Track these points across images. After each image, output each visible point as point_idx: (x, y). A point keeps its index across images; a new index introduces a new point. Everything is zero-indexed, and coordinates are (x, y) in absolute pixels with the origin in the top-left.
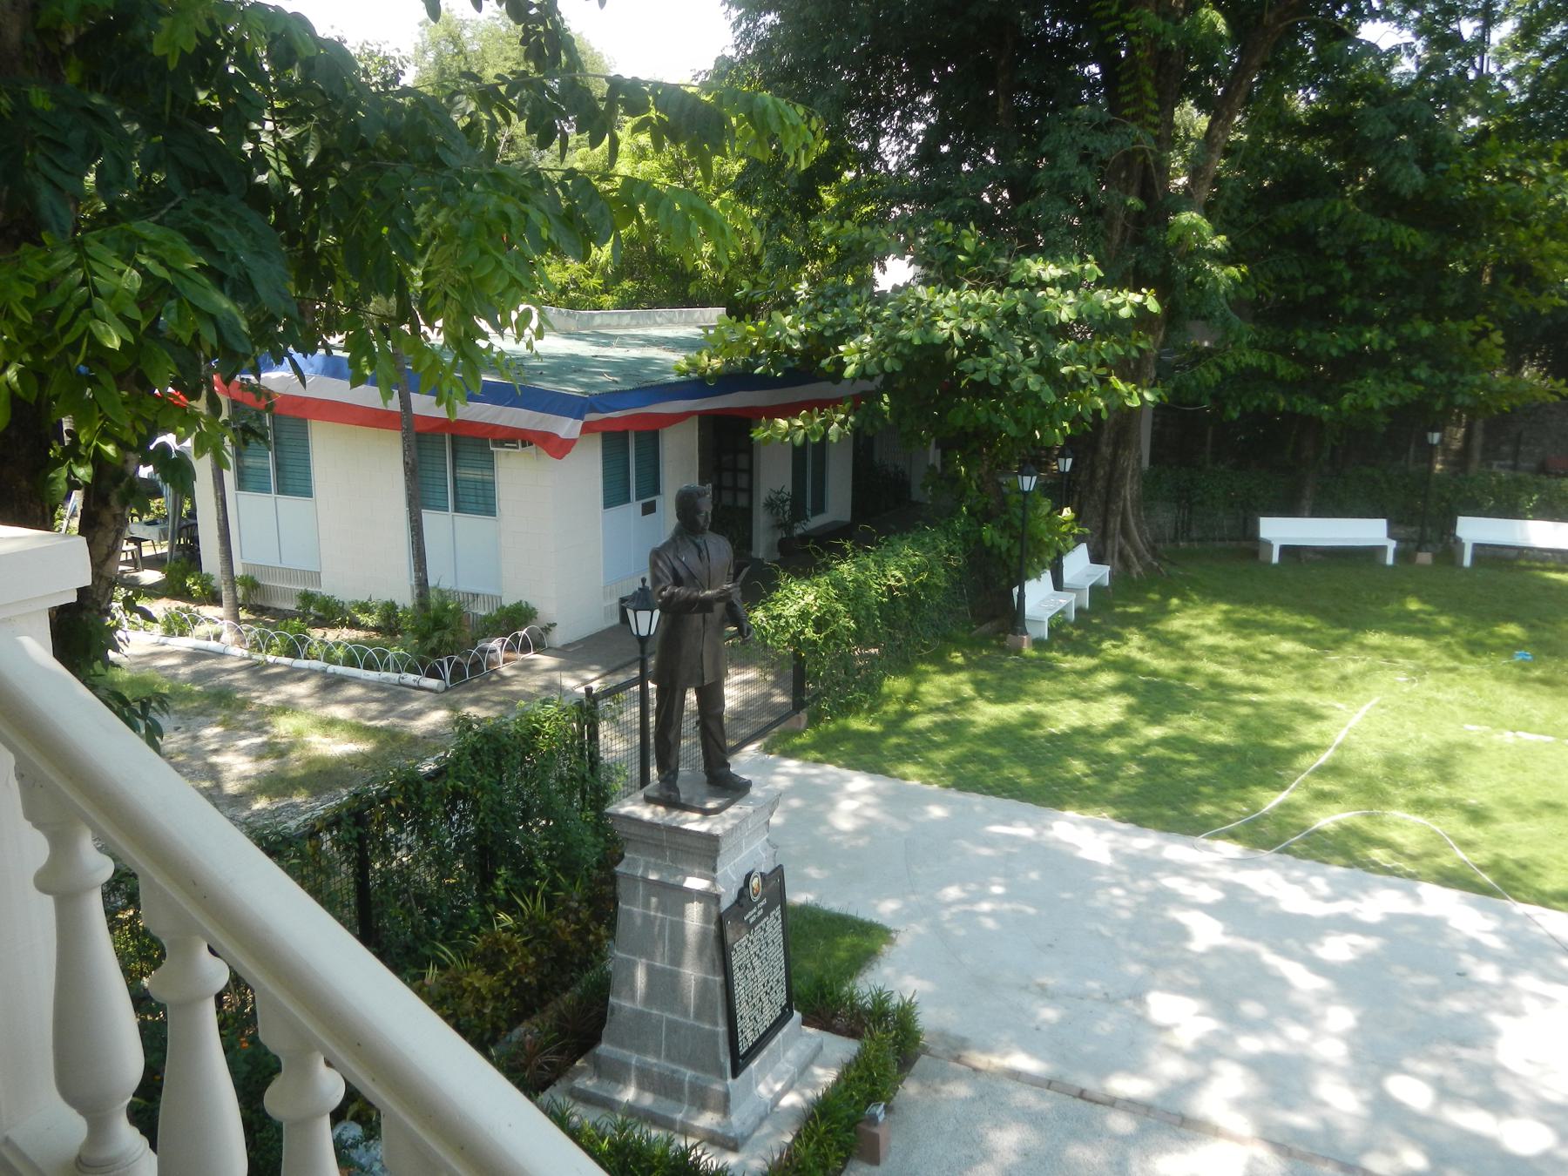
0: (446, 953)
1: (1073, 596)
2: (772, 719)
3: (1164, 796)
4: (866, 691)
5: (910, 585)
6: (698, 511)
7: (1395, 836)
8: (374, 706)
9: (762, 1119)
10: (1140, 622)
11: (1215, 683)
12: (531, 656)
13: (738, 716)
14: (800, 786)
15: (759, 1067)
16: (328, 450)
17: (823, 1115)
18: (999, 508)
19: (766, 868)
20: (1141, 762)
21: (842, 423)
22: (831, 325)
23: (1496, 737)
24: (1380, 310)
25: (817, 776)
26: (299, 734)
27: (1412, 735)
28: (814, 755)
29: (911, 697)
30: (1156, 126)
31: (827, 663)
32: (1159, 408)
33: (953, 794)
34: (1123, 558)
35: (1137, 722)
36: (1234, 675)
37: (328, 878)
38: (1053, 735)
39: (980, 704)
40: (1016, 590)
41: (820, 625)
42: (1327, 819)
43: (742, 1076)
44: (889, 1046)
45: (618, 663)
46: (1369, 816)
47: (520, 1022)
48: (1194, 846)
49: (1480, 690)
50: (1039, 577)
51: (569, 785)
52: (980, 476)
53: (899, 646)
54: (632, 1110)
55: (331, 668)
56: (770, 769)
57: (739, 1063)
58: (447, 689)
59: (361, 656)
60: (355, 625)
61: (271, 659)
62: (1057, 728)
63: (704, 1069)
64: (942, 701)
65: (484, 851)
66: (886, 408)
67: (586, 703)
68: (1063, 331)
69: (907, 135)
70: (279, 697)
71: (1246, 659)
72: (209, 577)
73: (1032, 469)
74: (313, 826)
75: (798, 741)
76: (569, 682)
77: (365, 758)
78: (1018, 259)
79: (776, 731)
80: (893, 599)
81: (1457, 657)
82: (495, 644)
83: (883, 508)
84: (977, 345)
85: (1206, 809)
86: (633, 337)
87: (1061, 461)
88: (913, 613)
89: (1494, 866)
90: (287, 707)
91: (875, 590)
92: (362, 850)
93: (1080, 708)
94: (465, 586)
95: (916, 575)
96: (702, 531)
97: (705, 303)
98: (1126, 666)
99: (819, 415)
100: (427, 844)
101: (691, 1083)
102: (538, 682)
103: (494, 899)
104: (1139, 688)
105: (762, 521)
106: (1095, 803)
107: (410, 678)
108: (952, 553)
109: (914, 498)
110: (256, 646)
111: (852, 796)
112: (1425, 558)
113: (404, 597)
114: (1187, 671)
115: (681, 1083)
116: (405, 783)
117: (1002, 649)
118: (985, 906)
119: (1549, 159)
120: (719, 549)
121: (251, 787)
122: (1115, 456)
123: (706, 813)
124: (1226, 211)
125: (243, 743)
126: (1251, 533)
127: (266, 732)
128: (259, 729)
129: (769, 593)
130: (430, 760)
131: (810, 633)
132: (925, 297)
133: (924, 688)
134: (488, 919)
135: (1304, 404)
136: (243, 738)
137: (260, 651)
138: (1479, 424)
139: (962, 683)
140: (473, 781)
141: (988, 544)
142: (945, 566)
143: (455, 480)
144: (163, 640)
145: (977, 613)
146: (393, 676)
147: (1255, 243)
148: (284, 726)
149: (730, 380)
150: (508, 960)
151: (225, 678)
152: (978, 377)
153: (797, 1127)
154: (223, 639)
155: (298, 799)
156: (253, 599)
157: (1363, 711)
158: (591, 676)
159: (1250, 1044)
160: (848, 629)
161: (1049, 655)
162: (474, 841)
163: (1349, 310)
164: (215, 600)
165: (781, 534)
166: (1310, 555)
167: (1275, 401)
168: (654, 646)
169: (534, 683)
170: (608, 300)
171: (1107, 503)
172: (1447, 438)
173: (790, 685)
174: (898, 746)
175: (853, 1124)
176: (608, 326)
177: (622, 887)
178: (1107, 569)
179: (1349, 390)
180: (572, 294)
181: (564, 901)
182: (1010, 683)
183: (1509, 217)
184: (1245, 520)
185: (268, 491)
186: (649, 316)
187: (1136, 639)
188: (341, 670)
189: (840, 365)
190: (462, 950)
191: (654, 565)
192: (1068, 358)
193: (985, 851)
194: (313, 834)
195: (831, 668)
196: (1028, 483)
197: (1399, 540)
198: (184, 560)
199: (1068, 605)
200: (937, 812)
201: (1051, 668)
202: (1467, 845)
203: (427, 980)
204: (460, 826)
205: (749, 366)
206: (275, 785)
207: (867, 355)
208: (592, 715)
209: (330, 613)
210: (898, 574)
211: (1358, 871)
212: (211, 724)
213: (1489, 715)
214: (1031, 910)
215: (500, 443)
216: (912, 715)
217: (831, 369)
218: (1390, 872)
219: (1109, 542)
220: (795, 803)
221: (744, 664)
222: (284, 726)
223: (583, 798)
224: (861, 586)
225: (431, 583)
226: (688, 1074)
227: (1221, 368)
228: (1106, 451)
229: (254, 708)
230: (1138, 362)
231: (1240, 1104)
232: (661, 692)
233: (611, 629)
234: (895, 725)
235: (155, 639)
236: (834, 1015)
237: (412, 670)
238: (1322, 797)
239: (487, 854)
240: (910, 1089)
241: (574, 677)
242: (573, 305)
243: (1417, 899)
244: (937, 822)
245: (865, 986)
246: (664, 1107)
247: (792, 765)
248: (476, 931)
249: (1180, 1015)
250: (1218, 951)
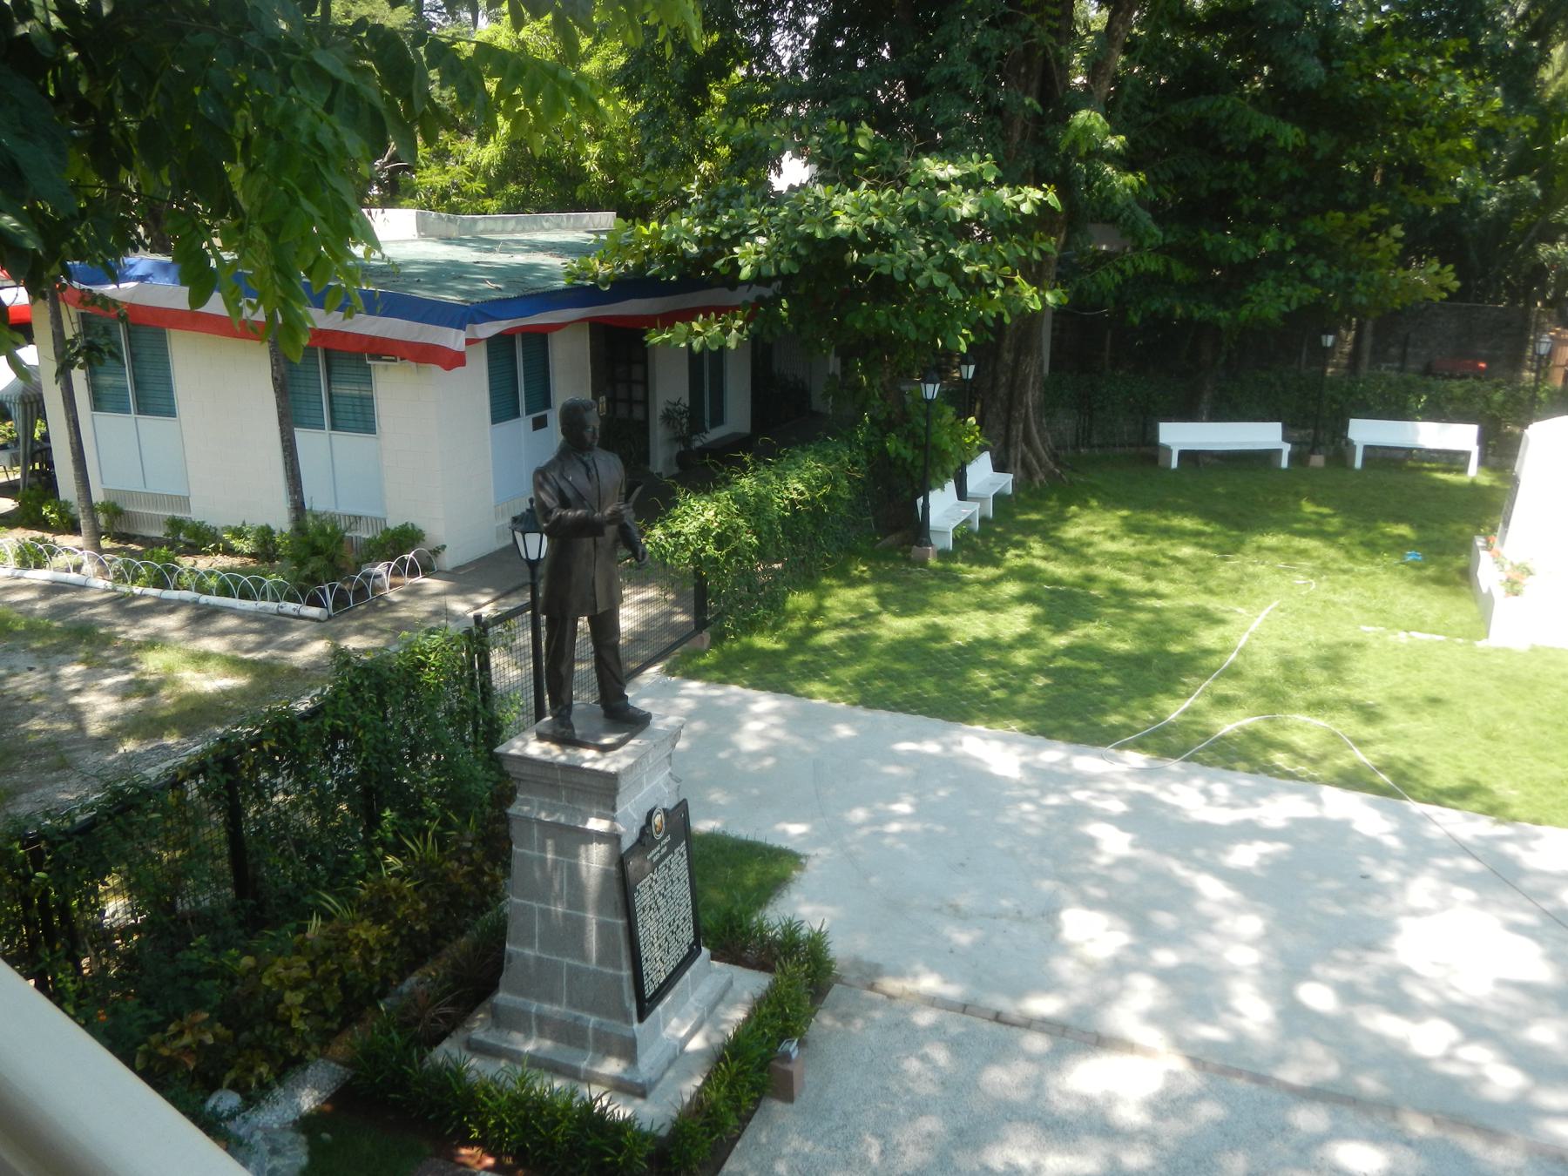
0: (330, 901)
1: (977, 506)
2: (674, 639)
3: (1072, 705)
4: (770, 607)
5: (813, 498)
6: (584, 426)
7: (1298, 739)
8: (251, 638)
9: (671, 1062)
10: (1045, 533)
12: (419, 580)
13: (638, 638)
14: (704, 709)
15: (666, 1009)
16: (192, 364)
17: (734, 1057)
18: (898, 420)
19: (669, 804)
20: (1047, 673)
21: (740, 330)
22: (728, 227)
23: (1391, 638)
24: (1277, 210)
25: (720, 697)
26: (170, 669)
27: (1311, 638)
28: (716, 675)
29: (818, 612)
30: (1056, 19)
31: (729, 581)
32: (1060, 313)
33: (860, 712)
34: (1025, 465)
35: (1044, 633)
36: (1133, 581)
37: (196, 830)
38: (960, 647)
39: (886, 618)
40: (920, 501)
41: (721, 541)
42: (1228, 724)
43: (649, 1020)
44: (801, 980)
45: (511, 585)
46: (1271, 721)
47: (412, 971)
48: (1102, 757)
49: (1374, 591)
50: (943, 488)
51: (459, 718)
52: (882, 385)
53: (803, 561)
54: (536, 1062)
55: (204, 599)
56: (673, 691)
57: (645, 1006)
58: (330, 617)
59: (236, 584)
60: (230, 551)
61: (137, 590)
62: (959, 640)
63: (609, 1015)
64: (847, 616)
65: (367, 792)
66: (784, 314)
67: (475, 631)
68: (961, 230)
69: (800, 29)
70: (147, 631)
71: (1150, 566)
72: (67, 504)
73: (936, 376)
74: (176, 775)
75: (702, 662)
76: (459, 606)
77: (242, 694)
78: (916, 157)
79: (676, 650)
80: (796, 513)
81: (1352, 557)
82: (381, 568)
83: (783, 421)
84: (878, 240)
85: (1115, 719)
86: (518, 242)
87: (964, 367)
88: (816, 526)
89: (1387, 766)
90: (154, 642)
91: (778, 503)
92: (233, 796)
93: (987, 618)
94: (346, 507)
95: (819, 488)
96: (590, 448)
97: (595, 207)
98: (1026, 574)
99: (717, 321)
100: (306, 787)
101: (596, 1030)
102: (430, 608)
103: (382, 842)
104: (1044, 597)
105: (659, 434)
106: (1004, 716)
107: (290, 607)
108: (855, 463)
109: (814, 408)
110: (120, 577)
111: (757, 717)
112: (1318, 460)
113: (280, 520)
114: (1090, 579)
115: (584, 1030)
116: (278, 724)
117: (908, 560)
118: (895, 827)
119: (1441, 56)
120: (609, 468)
121: (118, 729)
122: (1016, 362)
123: (604, 749)
124: (1126, 108)
125: (108, 682)
127: (133, 669)
128: (125, 666)
129: (668, 510)
130: (307, 699)
131: (710, 549)
132: (823, 196)
133: (828, 603)
134: (375, 864)
135: (1204, 311)
136: (107, 676)
137: (125, 581)
138: (1369, 326)
139: (867, 596)
140: (354, 720)
141: (893, 455)
142: (849, 478)
143: (331, 396)
144: (18, 573)
145: (880, 526)
147: (1154, 143)
148: (153, 663)
149: (626, 286)
150: (396, 908)
151: (87, 612)
152: (885, 270)
153: (708, 1068)
154: (84, 569)
155: (170, 741)
156: (115, 525)
157: (1263, 615)
158: (483, 600)
159: (1166, 957)
160: (750, 545)
161: (953, 566)
162: (357, 782)
163: (1246, 210)
164: (73, 528)
166: (1208, 460)
168: (542, 570)
169: (423, 608)
170: (492, 204)
171: (1009, 410)
172: (1338, 342)
173: (691, 604)
174: (804, 663)
175: (764, 1064)
176: (492, 231)
177: (515, 831)
178: (1011, 476)
180: (454, 199)
181: (456, 842)
182: (914, 595)
183: (1403, 116)
185: (127, 411)
186: (535, 221)
187: (1037, 548)
188: (214, 600)
189: (735, 267)
190: (347, 897)
191: (539, 486)
192: (969, 259)
193: (894, 770)
194: (175, 783)
195: (733, 586)
196: (931, 391)
197: (1294, 444)
198: (39, 487)
199: (973, 514)
200: (844, 731)
201: (957, 579)
202: (1360, 743)
203: (309, 934)
204: (341, 767)
205: (641, 268)
206: (144, 725)
207: (763, 256)
208: (481, 644)
209: (200, 539)
210: (800, 487)
211: (1263, 777)
212: (72, 662)
213: (1383, 616)
214: (940, 828)
215: (378, 357)
216: (818, 631)
217: (725, 271)
218: (1291, 776)
219: (1012, 451)
220: (697, 726)
221: (642, 583)
222: (153, 663)
223: (475, 731)
224: (763, 501)
226: (592, 1020)
227: (1122, 272)
228: (1008, 357)
229: (119, 643)
230: (1039, 264)
231: (1152, 1018)
232: (551, 623)
234: (799, 642)
235: (8, 572)
236: (744, 949)
237: (292, 598)
238: (1224, 702)
239: (371, 794)
240: (825, 1020)
241: (466, 601)
242: (455, 210)
243: (1317, 801)
244: (844, 742)
245: (775, 916)
246: (565, 1055)
247: (694, 686)
248: (362, 876)
249: (1090, 933)
250: (1124, 863)
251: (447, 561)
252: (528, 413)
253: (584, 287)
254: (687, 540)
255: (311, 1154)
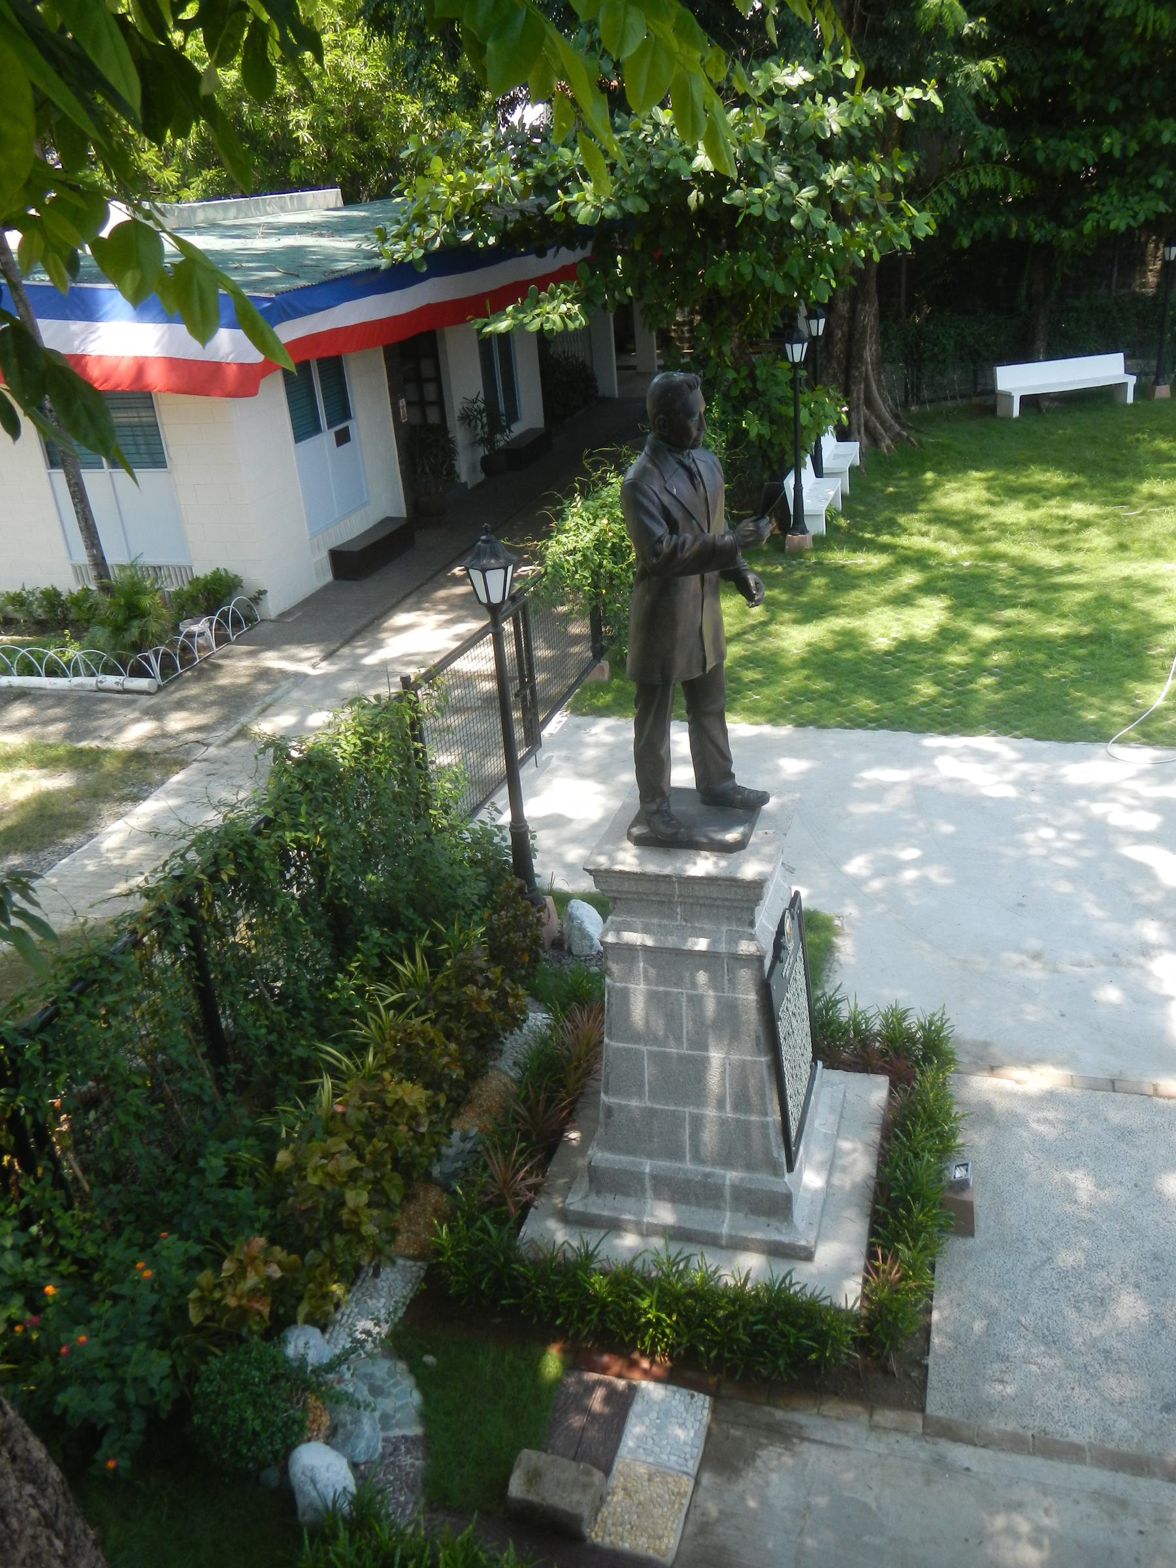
11: (1025, 568)
45: (352, 629)
59: (40, 660)
62: (882, 643)
87: (813, 323)
97: (307, 184)
107: (110, 681)
122: (853, 312)
126: (991, 391)
146: (90, 682)
152: (756, 211)
165: (482, 451)
167: (1008, 225)
179: (1091, 210)
184: (975, 372)
225: (110, 560)
227: (956, 193)
233: (326, 588)
251: (272, 607)
252: (330, 426)
253: (376, 269)
254: (584, 556)
255: (420, 1384)
